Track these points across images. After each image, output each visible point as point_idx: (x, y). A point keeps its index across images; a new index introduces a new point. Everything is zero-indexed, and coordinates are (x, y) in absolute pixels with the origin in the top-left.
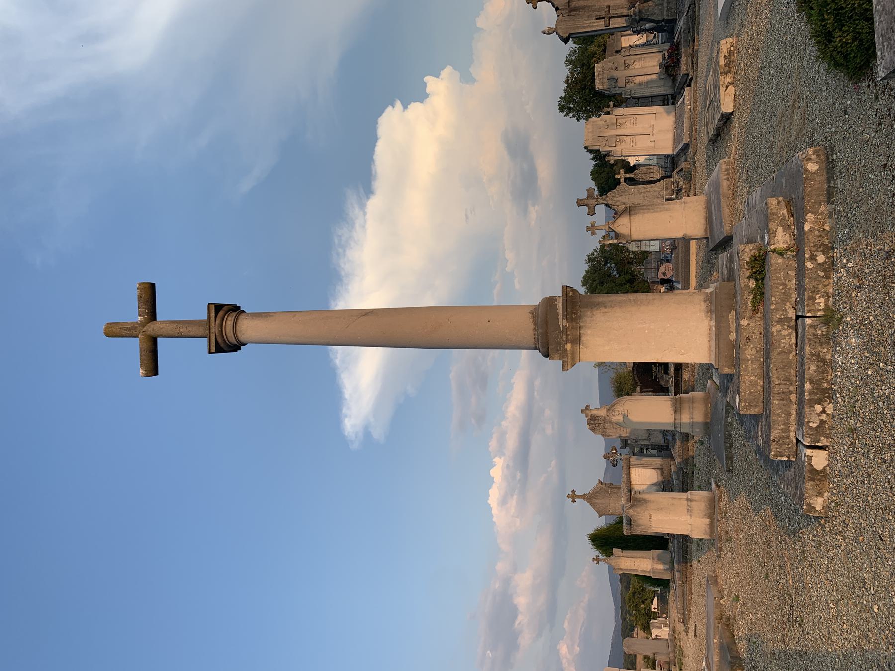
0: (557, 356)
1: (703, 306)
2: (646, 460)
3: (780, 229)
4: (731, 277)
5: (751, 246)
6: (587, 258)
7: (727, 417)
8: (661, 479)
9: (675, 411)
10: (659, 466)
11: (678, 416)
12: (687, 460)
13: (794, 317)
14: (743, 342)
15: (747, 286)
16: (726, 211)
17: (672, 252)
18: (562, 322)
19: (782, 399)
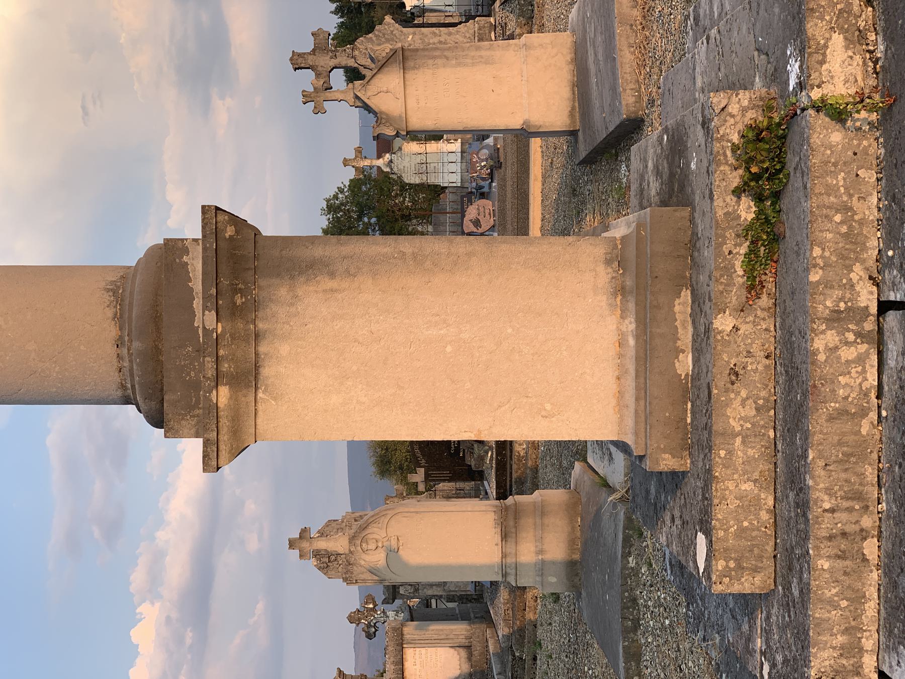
0: (189, 423)
1: (604, 275)
2: (436, 628)
3: (838, 40)
4: (677, 190)
5: (744, 97)
6: (324, 205)
7: (626, 555)
8: (466, 668)
9: (505, 537)
10: (462, 640)
11: (511, 548)
12: (521, 630)
13: (874, 309)
14: (720, 380)
15: (732, 216)
16: (627, 58)
17: (491, 175)
18: (206, 320)
19: (842, 556)
